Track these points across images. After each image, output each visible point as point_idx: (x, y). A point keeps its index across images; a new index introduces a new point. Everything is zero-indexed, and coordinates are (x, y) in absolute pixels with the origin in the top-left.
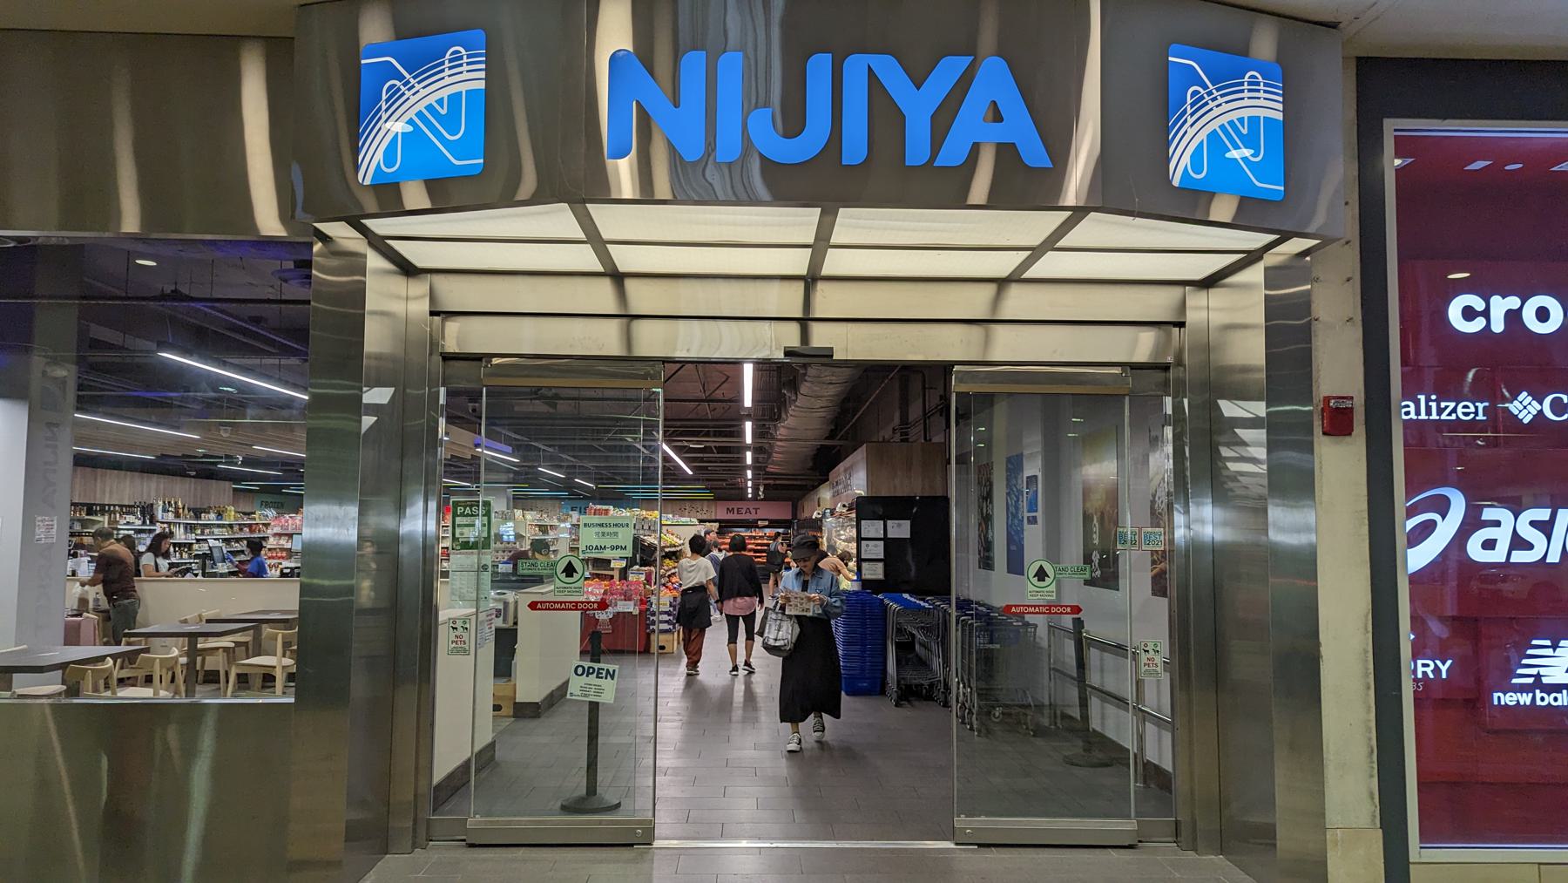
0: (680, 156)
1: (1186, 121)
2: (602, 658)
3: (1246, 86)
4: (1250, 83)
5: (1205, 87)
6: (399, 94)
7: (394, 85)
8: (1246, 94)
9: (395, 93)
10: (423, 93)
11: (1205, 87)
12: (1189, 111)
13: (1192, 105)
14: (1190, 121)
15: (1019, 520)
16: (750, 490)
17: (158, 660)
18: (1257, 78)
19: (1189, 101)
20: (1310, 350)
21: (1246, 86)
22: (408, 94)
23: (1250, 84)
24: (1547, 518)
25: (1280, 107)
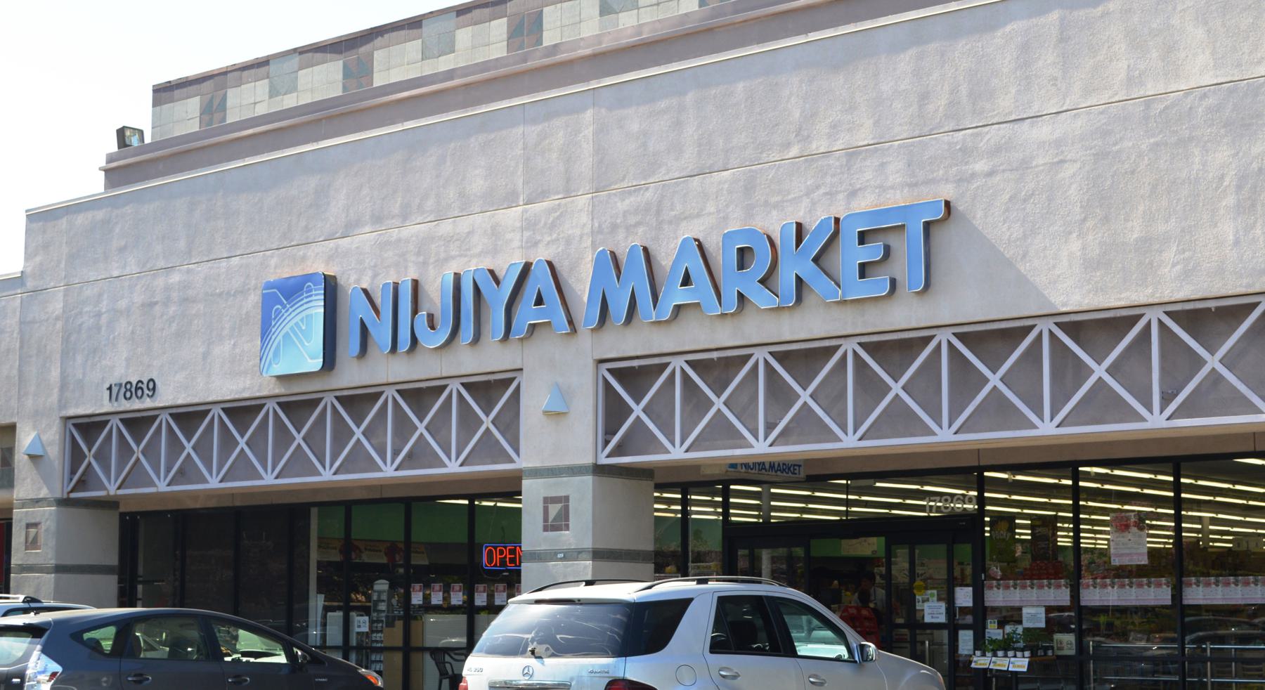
1: (271, 331)
5: (282, 304)
11: (282, 304)
22: (283, 311)
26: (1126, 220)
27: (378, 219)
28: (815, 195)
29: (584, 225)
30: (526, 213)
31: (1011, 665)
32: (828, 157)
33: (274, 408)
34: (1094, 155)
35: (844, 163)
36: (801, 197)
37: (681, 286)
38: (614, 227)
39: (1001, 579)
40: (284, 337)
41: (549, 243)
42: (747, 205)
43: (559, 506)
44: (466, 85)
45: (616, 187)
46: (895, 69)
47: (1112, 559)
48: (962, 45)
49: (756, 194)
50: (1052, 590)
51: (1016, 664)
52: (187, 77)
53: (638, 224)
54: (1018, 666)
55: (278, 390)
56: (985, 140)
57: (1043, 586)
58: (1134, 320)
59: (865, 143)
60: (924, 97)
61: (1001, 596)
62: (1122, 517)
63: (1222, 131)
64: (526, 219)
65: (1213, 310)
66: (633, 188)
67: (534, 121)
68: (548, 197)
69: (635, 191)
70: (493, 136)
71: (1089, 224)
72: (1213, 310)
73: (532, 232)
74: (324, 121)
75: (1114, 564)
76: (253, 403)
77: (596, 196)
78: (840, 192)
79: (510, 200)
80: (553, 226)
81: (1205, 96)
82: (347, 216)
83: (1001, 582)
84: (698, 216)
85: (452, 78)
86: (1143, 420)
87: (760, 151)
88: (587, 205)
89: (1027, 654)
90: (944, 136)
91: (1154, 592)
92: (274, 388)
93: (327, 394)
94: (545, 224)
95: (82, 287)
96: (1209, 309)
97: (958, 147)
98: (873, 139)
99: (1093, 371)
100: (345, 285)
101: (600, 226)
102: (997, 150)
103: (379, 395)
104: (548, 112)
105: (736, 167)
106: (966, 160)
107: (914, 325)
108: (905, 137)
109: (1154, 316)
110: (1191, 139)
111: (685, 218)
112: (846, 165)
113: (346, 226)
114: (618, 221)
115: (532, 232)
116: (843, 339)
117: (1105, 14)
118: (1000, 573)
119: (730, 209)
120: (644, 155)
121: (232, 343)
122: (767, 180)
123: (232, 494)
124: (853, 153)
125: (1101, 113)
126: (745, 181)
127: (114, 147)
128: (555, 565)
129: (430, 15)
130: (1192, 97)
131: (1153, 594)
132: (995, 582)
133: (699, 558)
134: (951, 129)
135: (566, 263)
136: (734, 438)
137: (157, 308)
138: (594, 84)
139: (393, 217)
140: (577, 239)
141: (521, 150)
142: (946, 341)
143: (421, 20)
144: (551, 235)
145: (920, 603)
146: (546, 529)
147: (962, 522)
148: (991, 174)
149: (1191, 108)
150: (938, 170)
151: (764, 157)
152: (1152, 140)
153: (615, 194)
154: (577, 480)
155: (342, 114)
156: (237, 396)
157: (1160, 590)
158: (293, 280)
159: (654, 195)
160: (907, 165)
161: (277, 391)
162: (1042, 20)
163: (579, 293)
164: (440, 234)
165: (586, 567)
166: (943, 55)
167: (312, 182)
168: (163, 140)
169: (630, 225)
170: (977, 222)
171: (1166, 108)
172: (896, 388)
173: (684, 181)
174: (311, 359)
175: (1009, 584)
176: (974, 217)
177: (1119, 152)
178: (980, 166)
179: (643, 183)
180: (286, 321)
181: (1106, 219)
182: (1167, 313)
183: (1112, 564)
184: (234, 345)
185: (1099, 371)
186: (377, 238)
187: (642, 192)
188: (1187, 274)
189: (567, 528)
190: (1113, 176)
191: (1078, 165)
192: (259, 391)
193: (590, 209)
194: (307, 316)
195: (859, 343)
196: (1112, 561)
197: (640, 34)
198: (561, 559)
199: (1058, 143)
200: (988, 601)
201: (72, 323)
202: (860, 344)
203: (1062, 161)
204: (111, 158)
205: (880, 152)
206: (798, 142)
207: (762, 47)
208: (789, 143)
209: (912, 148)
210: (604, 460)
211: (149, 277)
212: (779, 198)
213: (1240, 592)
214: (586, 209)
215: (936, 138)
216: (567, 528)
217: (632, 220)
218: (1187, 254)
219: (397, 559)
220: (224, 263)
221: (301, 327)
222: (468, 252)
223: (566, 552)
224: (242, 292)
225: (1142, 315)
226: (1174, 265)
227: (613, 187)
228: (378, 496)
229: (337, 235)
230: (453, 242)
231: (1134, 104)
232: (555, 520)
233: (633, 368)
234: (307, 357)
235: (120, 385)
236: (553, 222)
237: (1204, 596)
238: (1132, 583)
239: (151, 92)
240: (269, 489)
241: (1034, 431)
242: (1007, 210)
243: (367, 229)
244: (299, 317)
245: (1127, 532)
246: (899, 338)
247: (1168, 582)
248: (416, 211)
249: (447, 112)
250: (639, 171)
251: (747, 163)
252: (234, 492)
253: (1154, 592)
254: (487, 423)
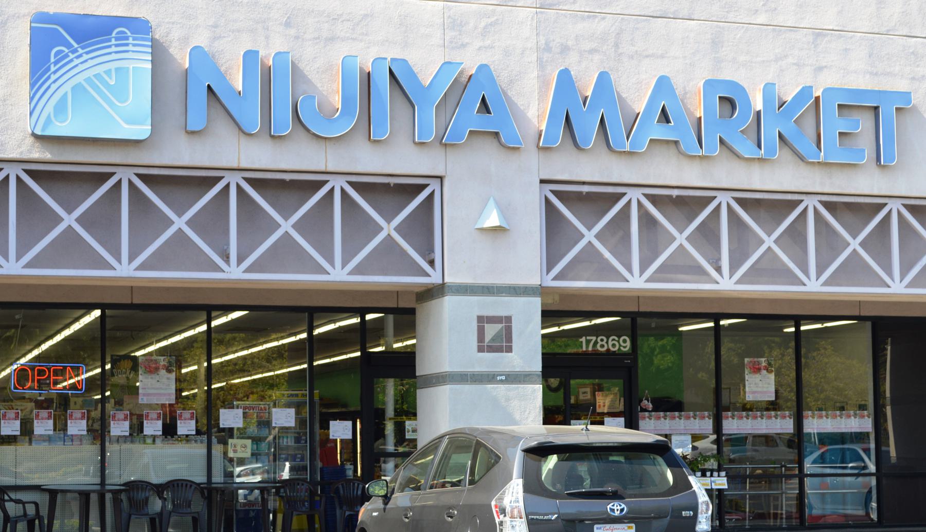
1: (49, 77)
3: (113, 42)
4: (117, 39)
5: (69, 46)
7: (62, 51)
8: (114, 49)
9: (60, 57)
10: (85, 57)
11: (69, 46)
12: (53, 69)
13: (56, 63)
15: (84, 359)
17: (787, 502)
18: (126, 33)
19: (52, 60)
21: (113, 42)
22: (72, 56)
30: (450, 10)
31: (713, 484)
32: (794, 31)
35: (812, 41)
37: (491, 114)
39: (652, 411)
41: (480, 49)
42: (715, 57)
43: (499, 326)
47: (747, 395)
49: (723, 49)
51: (717, 482)
53: (592, 51)
55: (38, 153)
57: (836, 416)
62: (755, 362)
64: (449, 17)
65: (392, 185)
72: (392, 185)
73: (458, 33)
75: (749, 400)
76: (610, 190)
77: (541, 13)
80: (485, 33)
83: (653, 413)
86: (112, 268)
87: (727, 10)
89: (723, 474)
90: (899, 38)
91: (780, 423)
94: (476, 28)
97: (911, 51)
101: (547, 44)
103: (618, 197)
105: (702, 19)
106: (918, 63)
107: (876, 193)
108: (865, 31)
111: (647, 56)
112: (813, 43)
114: (570, 43)
115: (458, 33)
116: (805, 195)
122: (735, 38)
123: (656, 297)
124: (819, 33)
126: (712, 34)
131: (779, 424)
132: (647, 413)
133: (565, 387)
134: (904, 34)
145: (410, 433)
146: (481, 349)
157: (703, 422)
159: (612, 26)
160: (868, 55)
163: (522, 108)
173: (646, 20)
174: (128, 123)
175: (689, 414)
182: (351, 184)
183: (747, 399)
185: (855, 244)
187: (597, 20)
189: (509, 349)
193: (535, 25)
195: (819, 201)
196: (747, 397)
198: (502, 381)
200: (725, 429)
205: (843, 39)
206: (766, 11)
208: (757, 11)
209: (872, 42)
210: (549, 282)
213: (653, 425)
215: (892, 39)
217: (587, 46)
219: (704, 374)
221: (107, 83)
223: (509, 375)
228: (127, 301)
230: (343, 21)
231: (787, 29)
232: (493, 340)
233: (581, 193)
236: (486, 27)
237: (767, 426)
238: (681, 415)
245: (759, 374)
246: (856, 201)
247: (710, 415)
253: (780, 423)
254: (389, 230)
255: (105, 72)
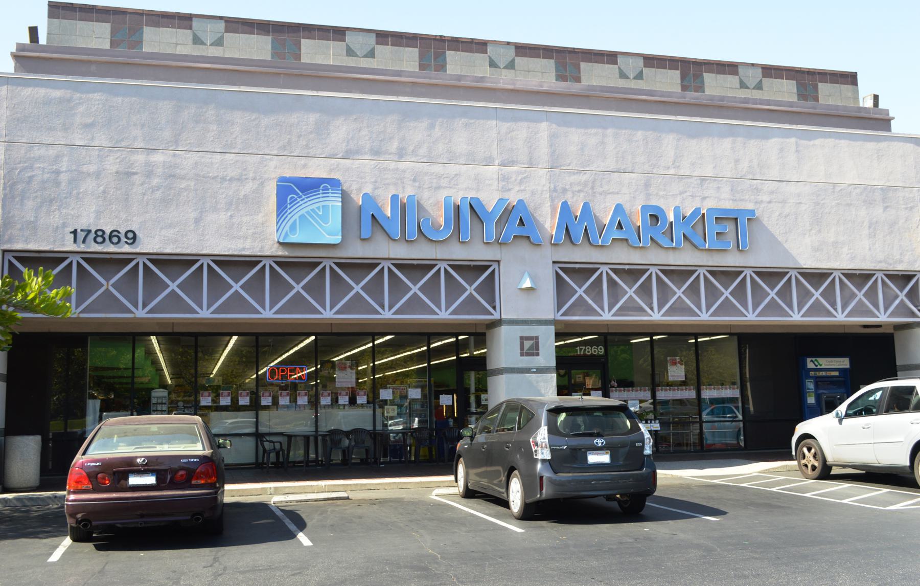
0: (277, 223)
1: (287, 211)
2: (592, 392)
3: (321, 191)
5: (297, 194)
6: (296, 202)
9: (293, 200)
11: (297, 194)
12: (289, 207)
14: (289, 207)
16: (195, 460)
18: (294, 197)
19: (289, 202)
20: (41, 476)
22: (299, 200)
23: (323, 190)
24: (848, 411)
25: (340, 196)
26: (828, 233)
27: (376, 153)
28: (684, 195)
29: (544, 185)
33: (656, 273)
34: (814, 203)
35: (699, 183)
36: (677, 195)
38: (565, 191)
39: (617, 387)
40: (300, 217)
43: (532, 342)
44: (413, 83)
45: (564, 168)
46: (722, 145)
48: (753, 142)
50: (671, 392)
52: (800, 68)
53: (579, 191)
54: (656, 428)
55: (281, 252)
56: (766, 187)
58: (194, 262)
59: (710, 175)
60: (737, 161)
61: (663, 394)
63: (863, 204)
66: (576, 171)
67: (504, 120)
68: (516, 165)
69: (577, 173)
70: (472, 121)
71: (813, 231)
73: (506, 183)
74: (282, 75)
78: (697, 196)
79: (488, 162)
80: (521, 182)
81: (855, 188)
82: (347, 146)
84: (618, 193)
85: (400, 76)
88: (545, 174)
92: (277, 251)
93: (878, 272)
94: (516, 180)
95: (33, 147)
96: (856, 274)
97: (754, 187)
98: (713, 174)
99: (820, 295)
100: (347, 190)
101: (555, 187)
102: (772, 192)
104: (515, 117)
107: (738, 265)
109: (386, 265)
110: (851, 204)
112: (700, 184)
113: (346, 152)
114: (567, 187)
117: (814, 145)
118: (616, 384)
119: (637, 194)
120: (582, 155)
121: (229, 214)
124: (703, 179)
125: (816, 186)
127: (26, 39)
128: (529, 376)
129: (353, 30)
130: (850, 187)
135: (532, 204)
136: (590, 311)
137: (137, 179)
138: (546, 109)
139: (390, 154)
140: (539, 192)
141: (495, 134)
142: (206, 264)
143: (345, 31)
144: (520, 186)
145: (484, 401)
146: (522, 355)
147: (602, 359)
148: (770, 202)
149: (850, 192)
150: (746, 196)
151: (655, 171)
152: (837, 202)
153: (564, 172)
154: (544, 327)
155: (128, 63)
156: (236, 253)
158: (310, 179)
161: (280, 253)
162: (788, 140)
163: (542, 223)
164: (433, 171)
165: (552, 377)
166: (744, 144)
167: (312, 118)
168: (379, 69)
169: (576, 191)
170: (765, 222)
171: (841, 190)
172: (727, 293)
174: (329, 235)
176: (763, 220)
177: (823, 204)
178: (766, 198)
179: (582, 169)
180: (301, 207)
181: (820, 231)
184: (231, 216)
185: (772, 294)
186: (376, 164)
187: (582, 174)
188: (853, 259)
189: (538, 355)
190: (821, 213)
191: (807, 206)
192: (260, 251)
194: (323, 206)
197: (542, 86)
198: (534, 372)
199: (799, 195)
201: (18, 174)
202: (707, 270)
203: (800, 203)
204: (21, 47)
207: (874, 133)
208: (669, 167)
211: (124, 153)
212: (665, 193)
214: (545, 177)
215: (744, 181)
216: (538, 355)
217: (576, 188)
218: (852, 251)
220: (218, 157)
222: (456, 186)
224: (238, 179)
225: (321, 263)
226: (847, 254)
227: (562, 168)
229: (338, 156)
232: (529, 349)
233: (575, 268)
234: (326, 235)
235: (89, 231)
236: (521, 180)
239: (47, 6)
240: (233, 321)
241: (198, 315)
242: (778, 220)
243: (366, 157)
244: (317, 205)
248: (411, 153)
249: (517, 104)
250: (579, 163)
251: (645, 172)
252: (609, 323)
254: (471, 290)
255: (317, 208)
